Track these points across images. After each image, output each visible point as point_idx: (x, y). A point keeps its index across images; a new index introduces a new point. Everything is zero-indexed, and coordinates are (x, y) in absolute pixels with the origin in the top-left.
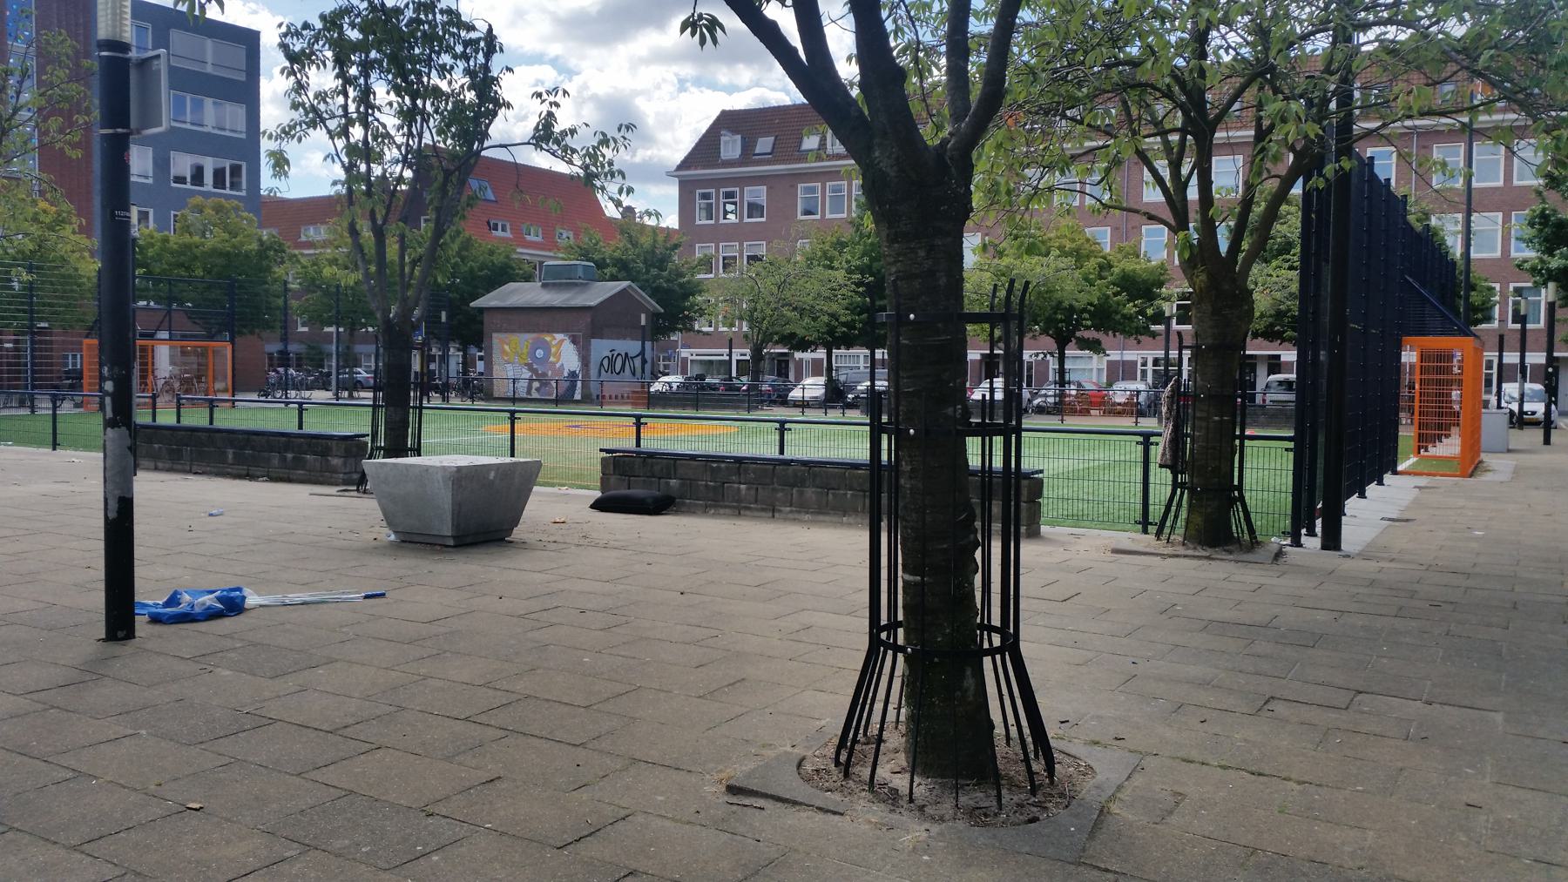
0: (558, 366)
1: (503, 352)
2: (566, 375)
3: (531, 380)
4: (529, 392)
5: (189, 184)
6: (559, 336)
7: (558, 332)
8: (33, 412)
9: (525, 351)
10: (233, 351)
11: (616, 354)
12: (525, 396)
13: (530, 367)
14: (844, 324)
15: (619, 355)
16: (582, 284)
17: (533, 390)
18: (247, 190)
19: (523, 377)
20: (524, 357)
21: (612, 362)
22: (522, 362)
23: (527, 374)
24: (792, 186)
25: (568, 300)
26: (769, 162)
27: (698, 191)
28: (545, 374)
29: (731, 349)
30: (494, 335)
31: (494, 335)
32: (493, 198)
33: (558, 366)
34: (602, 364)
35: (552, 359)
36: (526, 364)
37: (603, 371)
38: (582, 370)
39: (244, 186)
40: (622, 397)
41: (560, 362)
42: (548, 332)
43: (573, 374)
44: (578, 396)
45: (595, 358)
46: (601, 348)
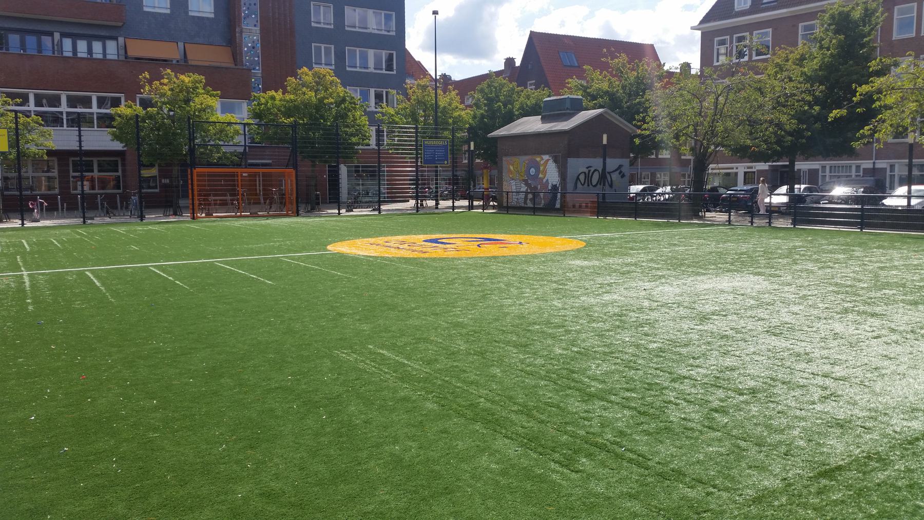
0: (544, 181)
1: (509, 171)
2: (550, 188)
3: (527, 193)
4: (525, 202)
5: (358, 68)
6: (546, 157)
7: (545, 154)
8: (380, 213)
9: (523, 170)
10: (297, 176)
11: (592, 170)
12: (523, 205)
13: (526, 182)
14: (790, 134)
15: (595, 170)
16: (569, 113)
17: (528, 201)
18: (335, 64)
19: (522, 190)
20: (522, 174)
21: (588, 177)
22: (522, 178)
23: (524, 188)
24: (794, 26)
25: (552, 127)
26: (774, 8)
27: (716, 39)
28: (536, 188)
29: (911, 159)
30: (504, 158)
31: (504, 158)
32: (576, 64)
33: (544, 181)
34: (578, 178)
35: (541, 176)
36: (524, 180)
37: (579, 184)
38: (561, 183)
39: (395, 68)
40: (580, 207)
41: (546, 178)
42: (538, 154)
43: (555, 187)
44: (558, 206)
45: (571, 173)
46: (578, 165)
